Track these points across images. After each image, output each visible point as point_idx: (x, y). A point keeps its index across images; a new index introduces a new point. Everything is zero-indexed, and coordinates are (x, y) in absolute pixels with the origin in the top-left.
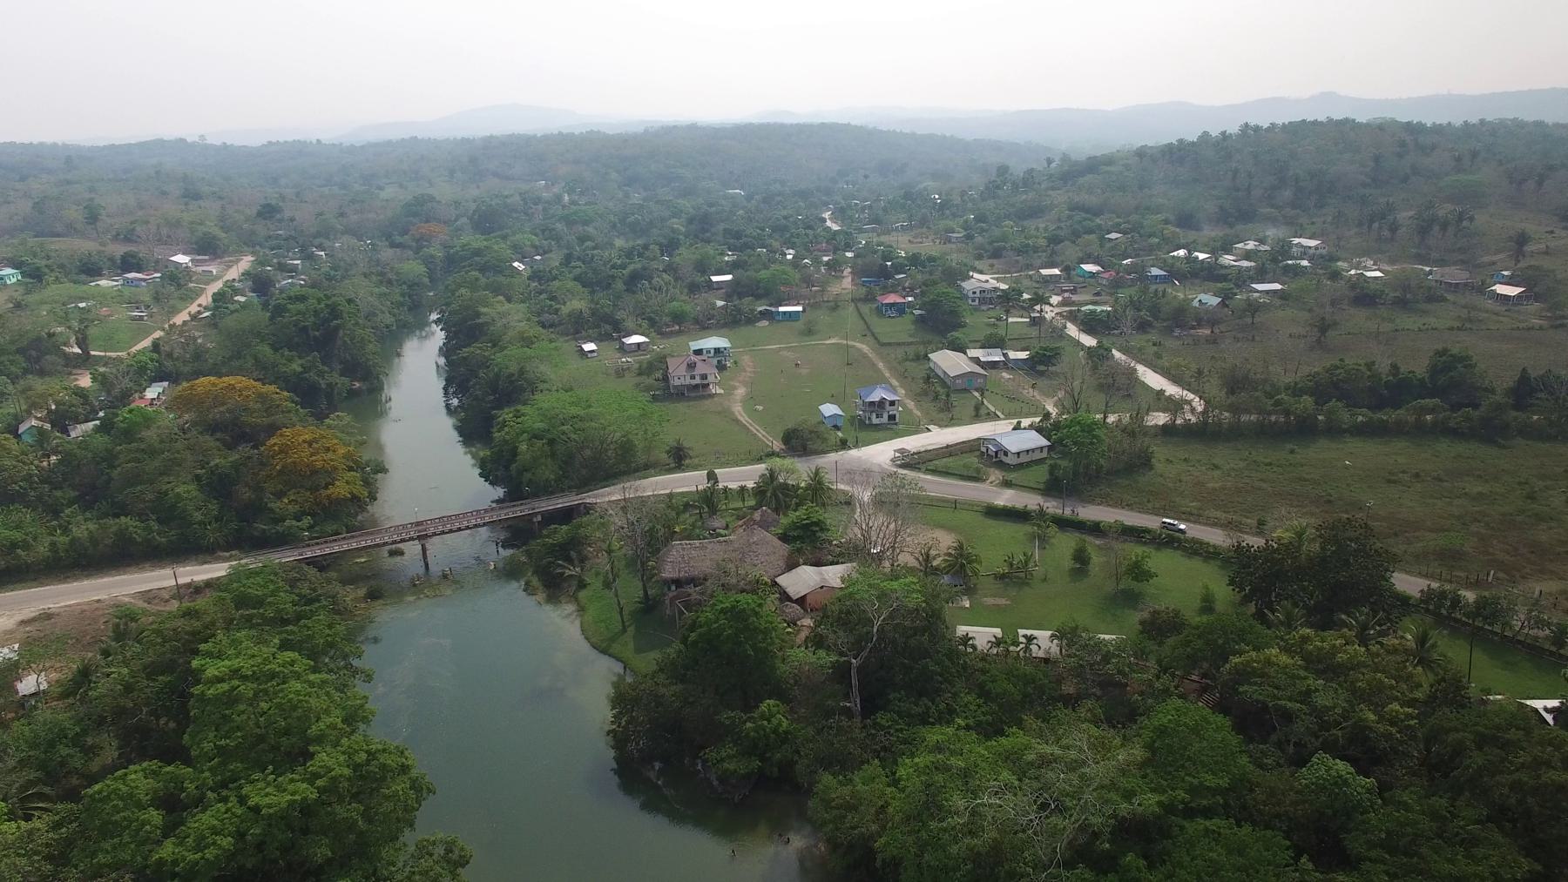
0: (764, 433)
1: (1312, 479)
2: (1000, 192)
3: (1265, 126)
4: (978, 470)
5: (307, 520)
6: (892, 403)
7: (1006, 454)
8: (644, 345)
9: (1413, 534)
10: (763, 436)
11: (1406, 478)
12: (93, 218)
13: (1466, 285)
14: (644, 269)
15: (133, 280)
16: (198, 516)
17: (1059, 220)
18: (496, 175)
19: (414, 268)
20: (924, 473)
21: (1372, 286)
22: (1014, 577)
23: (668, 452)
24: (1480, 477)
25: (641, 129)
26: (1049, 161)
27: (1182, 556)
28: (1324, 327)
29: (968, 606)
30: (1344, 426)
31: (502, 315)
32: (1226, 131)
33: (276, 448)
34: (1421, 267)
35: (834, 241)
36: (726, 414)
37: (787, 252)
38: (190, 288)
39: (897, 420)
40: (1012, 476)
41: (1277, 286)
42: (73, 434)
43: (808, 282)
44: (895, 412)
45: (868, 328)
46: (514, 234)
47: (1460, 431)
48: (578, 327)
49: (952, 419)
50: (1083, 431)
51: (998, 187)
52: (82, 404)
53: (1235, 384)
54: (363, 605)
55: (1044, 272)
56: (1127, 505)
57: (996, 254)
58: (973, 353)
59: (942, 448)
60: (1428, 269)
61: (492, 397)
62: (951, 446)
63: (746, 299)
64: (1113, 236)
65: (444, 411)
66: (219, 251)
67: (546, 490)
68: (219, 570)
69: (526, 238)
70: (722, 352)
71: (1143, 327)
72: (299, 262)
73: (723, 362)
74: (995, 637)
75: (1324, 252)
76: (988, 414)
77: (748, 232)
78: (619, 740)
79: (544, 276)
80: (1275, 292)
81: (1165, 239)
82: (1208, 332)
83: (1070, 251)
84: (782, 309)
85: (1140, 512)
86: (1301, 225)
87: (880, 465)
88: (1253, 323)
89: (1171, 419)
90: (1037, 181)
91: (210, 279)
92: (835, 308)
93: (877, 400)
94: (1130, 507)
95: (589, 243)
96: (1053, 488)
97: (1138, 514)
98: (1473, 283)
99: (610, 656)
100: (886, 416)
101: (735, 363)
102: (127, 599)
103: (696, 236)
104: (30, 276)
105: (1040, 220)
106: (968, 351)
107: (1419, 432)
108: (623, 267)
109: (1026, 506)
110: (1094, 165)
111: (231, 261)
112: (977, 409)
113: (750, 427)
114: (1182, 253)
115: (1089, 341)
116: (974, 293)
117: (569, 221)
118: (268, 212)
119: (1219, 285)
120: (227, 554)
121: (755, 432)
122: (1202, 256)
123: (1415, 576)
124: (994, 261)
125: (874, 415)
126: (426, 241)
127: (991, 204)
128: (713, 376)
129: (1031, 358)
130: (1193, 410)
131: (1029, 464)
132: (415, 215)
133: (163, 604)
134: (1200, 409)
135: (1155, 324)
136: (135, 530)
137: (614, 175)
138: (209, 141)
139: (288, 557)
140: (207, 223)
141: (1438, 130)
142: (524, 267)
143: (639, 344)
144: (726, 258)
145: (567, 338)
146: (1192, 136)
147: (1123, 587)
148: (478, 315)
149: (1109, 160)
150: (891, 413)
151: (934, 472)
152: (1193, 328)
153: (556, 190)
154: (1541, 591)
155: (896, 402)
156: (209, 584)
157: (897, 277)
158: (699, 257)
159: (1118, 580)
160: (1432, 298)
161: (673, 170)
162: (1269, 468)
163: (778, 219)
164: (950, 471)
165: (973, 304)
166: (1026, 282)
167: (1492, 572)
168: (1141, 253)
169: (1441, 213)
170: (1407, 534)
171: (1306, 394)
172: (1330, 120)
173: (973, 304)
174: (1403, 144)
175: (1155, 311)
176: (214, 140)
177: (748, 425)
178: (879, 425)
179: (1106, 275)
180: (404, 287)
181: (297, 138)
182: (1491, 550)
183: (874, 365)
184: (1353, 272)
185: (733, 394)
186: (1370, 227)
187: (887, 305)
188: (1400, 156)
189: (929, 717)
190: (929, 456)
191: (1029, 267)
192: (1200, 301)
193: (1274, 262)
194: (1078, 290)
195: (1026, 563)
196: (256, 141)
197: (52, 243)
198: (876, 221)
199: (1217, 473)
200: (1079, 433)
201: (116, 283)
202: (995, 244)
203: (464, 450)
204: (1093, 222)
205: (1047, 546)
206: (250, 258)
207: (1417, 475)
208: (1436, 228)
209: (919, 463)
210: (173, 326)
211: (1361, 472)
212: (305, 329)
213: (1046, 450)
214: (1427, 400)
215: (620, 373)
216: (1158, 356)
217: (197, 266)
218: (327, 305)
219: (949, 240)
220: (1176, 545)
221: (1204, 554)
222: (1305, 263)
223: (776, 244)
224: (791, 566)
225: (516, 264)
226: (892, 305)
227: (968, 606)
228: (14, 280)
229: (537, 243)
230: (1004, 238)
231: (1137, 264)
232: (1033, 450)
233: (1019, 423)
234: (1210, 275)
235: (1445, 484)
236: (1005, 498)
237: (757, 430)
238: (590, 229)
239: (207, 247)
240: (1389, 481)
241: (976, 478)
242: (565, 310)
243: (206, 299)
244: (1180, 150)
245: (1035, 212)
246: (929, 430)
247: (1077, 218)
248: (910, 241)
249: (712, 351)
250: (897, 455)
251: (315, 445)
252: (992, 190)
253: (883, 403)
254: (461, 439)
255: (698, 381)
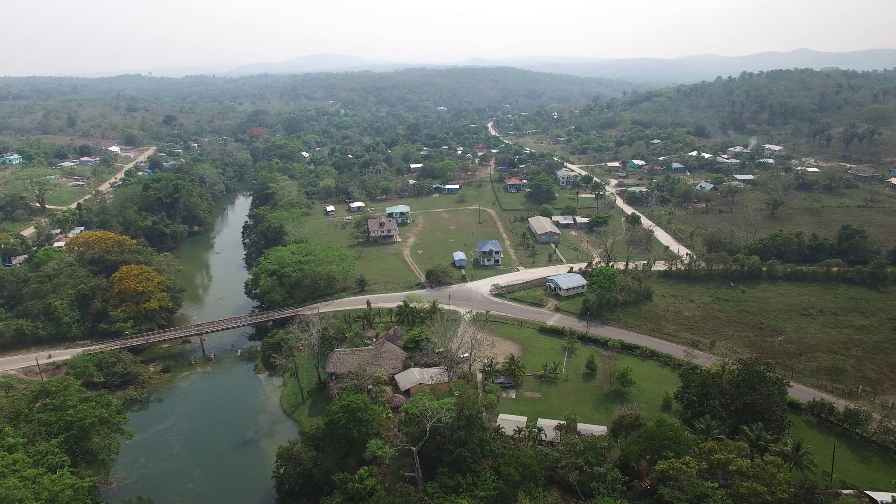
0: (418, 269)
1: (752, 311)
2: (592, 113)
3: (756, 73)
4: (541, 300)
5: (131, 323)
6: (497, 253)
7: (560, 289)
8: (362, 208)
9: (811, 355)
10: (417, 271)
11: (814, 313)
12: (72, 124)
13: (872, 177)
14: (371, 159)
15: (84, 162)
16: (66, 319)
17: (625, 131)
18: (306, 97)
19: (244, 155)
20: (508, 300)
21: (811, 178)
22: (547, 378)
23: (356, 282)
24: (863, 313)
25: (392, 70)
26: (625, 93)
27: (658, 366)
28: (775, 205)
29: (514, 397)
30: (780, 275)
31: (283, 188)
32: (731, 76)
33: (117, 278)
34: (844, 164)
35: (488, 143)
36: (400, 256)
37: (458, 149)
38: (117, 167)
39: (500, 263)
40: (562, 305)
41: (750, 177)
42: (14, 262)
43: (465, 169)
44: (498, 258)
45: (497, 200)
46: (305, 135)
47: (854, 280)
48: (327, 196)
49: (534, 262)
50: (605, 279)
51: (591, 109)
52: (20, 244)
53: (713, 245)
54: (158, 377)
55: (610, 164)
56: (630, 327)
57: (584, 152)
58: (555, 218)
59: (523, 283)
60: (849, 165)
61: (263, 242)
62: (529, 282)
63: (428, 179)
64: (655, 141)
65: (242, 246)
66: (137, 144)
67: (280, 306)
68: (66, 355)
69: (311, 138)
70: (405, 215)
71: (663, 201)
72: (181, 151)
73: (405, 221)
74: (517, 427)
75: (784, 153)
76: (557, 260)
77: (438, 136)
78: (280, 480)
79: (316, 162)
80: (749, 180)
81: (686, 145)
82: (704, 206)
83: (626, 151)
84: (447, 186)
85: (637, 332)
86: (772, 136)
87: (482, 294)
88: (733, 201)
89: (668, 268)
90: (615, 106)
91: (128, 160)
92: (480, 186)
93: (488, 250)
94: (631, 328)
95: (347, 141)
96: (588, 313)
97: (636, 334)
98: (877, 176)
99: (292, 419)
100: (493, 260)
101: (413, 221)
102: (13, 372)
103: (408, 139)
104: (26, 159)
105: (614, 130)
106: (552, 217)
107: (828, 279)
108: (361, 157)
109: (564, 328)
110: (650, 96)
111: (143, 150)
112: (550, 256)
113: (411, 265)
114: (694, 153)
115: (629, 210)
116: (564, 178)
117: (339, 127)
118: (169, 120)
119: (715, 175)
120: (82, 342)
121: (413, 268)
122: (707, 156)
123: (809, 387)
124: (583, 156)
125: (486, 260)
126: (256, 138)
127: (586, 119)
128: (395, 231)
129: (590, 222)
130: (682, 262)
131: (574, 296)
132: (253, 122)
133: (35, 375)
134: (686, 262)
135: (672, 199)
136: (27, 328)
137: (372, 98)
138: (154, 75)
139: (114, 345)
140: (134, 127)
141: (866, 75)
142: (308, 155)
143: (359, 208)
144: (422, 153)
145: (320, 202)
146: (711, 79)
147: (615, 387)
148: (269, 188)
149: (658, 94)
150: (496, 258)
151: (515, 300)
152: (696, 203)
153: (338, 106)
154: (893, 404)
155: (500, 252)
156: (65, 363)
157: (520, 166)
158: (405, 152)
159: (611, 384)
160: (849, 186)
161: (406, 95)
162: (725, 302)
163: (459, 128)
164: (524, 300)
165: (563, 184)
166: (598, 170)
167: (861, 387)
168: (671, 152)
169: (860, 131)
170: (808, 355)
171: (755, 254)
172: (797, 70)
173: (563, 184)
174: (840, 86)
175: (672, 191)
176: (158, 75)
177: (410, 264)
178: (488, 265)
179: (647, 167)
180: (237, 167)
181: (202, 73)
182: (863, 369)
183: (495, 224)
184: (799, 168)
185: (406, 242)
186: (814, 138)
187: (510, 185)
188: (838, 93)
189: (460, 488)
190: (514, 289)
191: (602, 161)
192: (701, 186)
193: (750, 162)
194: (629, 176)
195: (555, 369)
196: (179, 74)
197: (46, 138)
198: (517, 129)
199: (692, 305)
200: (602, 281)
201: (74, 164)
202: (583, 146)
203: (248, 272)
204: (643, 132)
205: (573, 356)
206: (155, 148)
207: (821, 311)
208: (856, 140)
209: (505, 294)
210: (98, 192)
211: (786, 308)
212: (160, 199)
213: (586, 288)
214: (833, 260)
215: (344, 226)
216: (669, 223)
217: (124, 152)
218: (173, 185)
219: (557, 142)
220: (655, 358)
221: (672, 366)
222: (771, 161)
223: (454, 144)
224: (406, 367)
225: (304, 153)
226: (513, 185)
227: (514, 397)
228: (18, 162)
229: (319, 140)
230: (588, 142)
231: (666, 160)
232: (577, 287)
233: (572, 268)
234: (711, 167)
235: (839, 318)
236: (554, 320)
237: (414, 267)
238: (349, 132)
239: (130, 142)
240: (802, 315)
241: (539, 305)
242: (322, 184)
243: (121, 175)
244: (701, 88)
245: (611, 125)
246: (518, 270)
247: (635, 130)
248: (535, 142)
249: (399, 214)
250: (493, 288)
251: (140, 277)
252: (587, 111)
253: (492, 252)
254: (246, 266)
255: (385, 234)
